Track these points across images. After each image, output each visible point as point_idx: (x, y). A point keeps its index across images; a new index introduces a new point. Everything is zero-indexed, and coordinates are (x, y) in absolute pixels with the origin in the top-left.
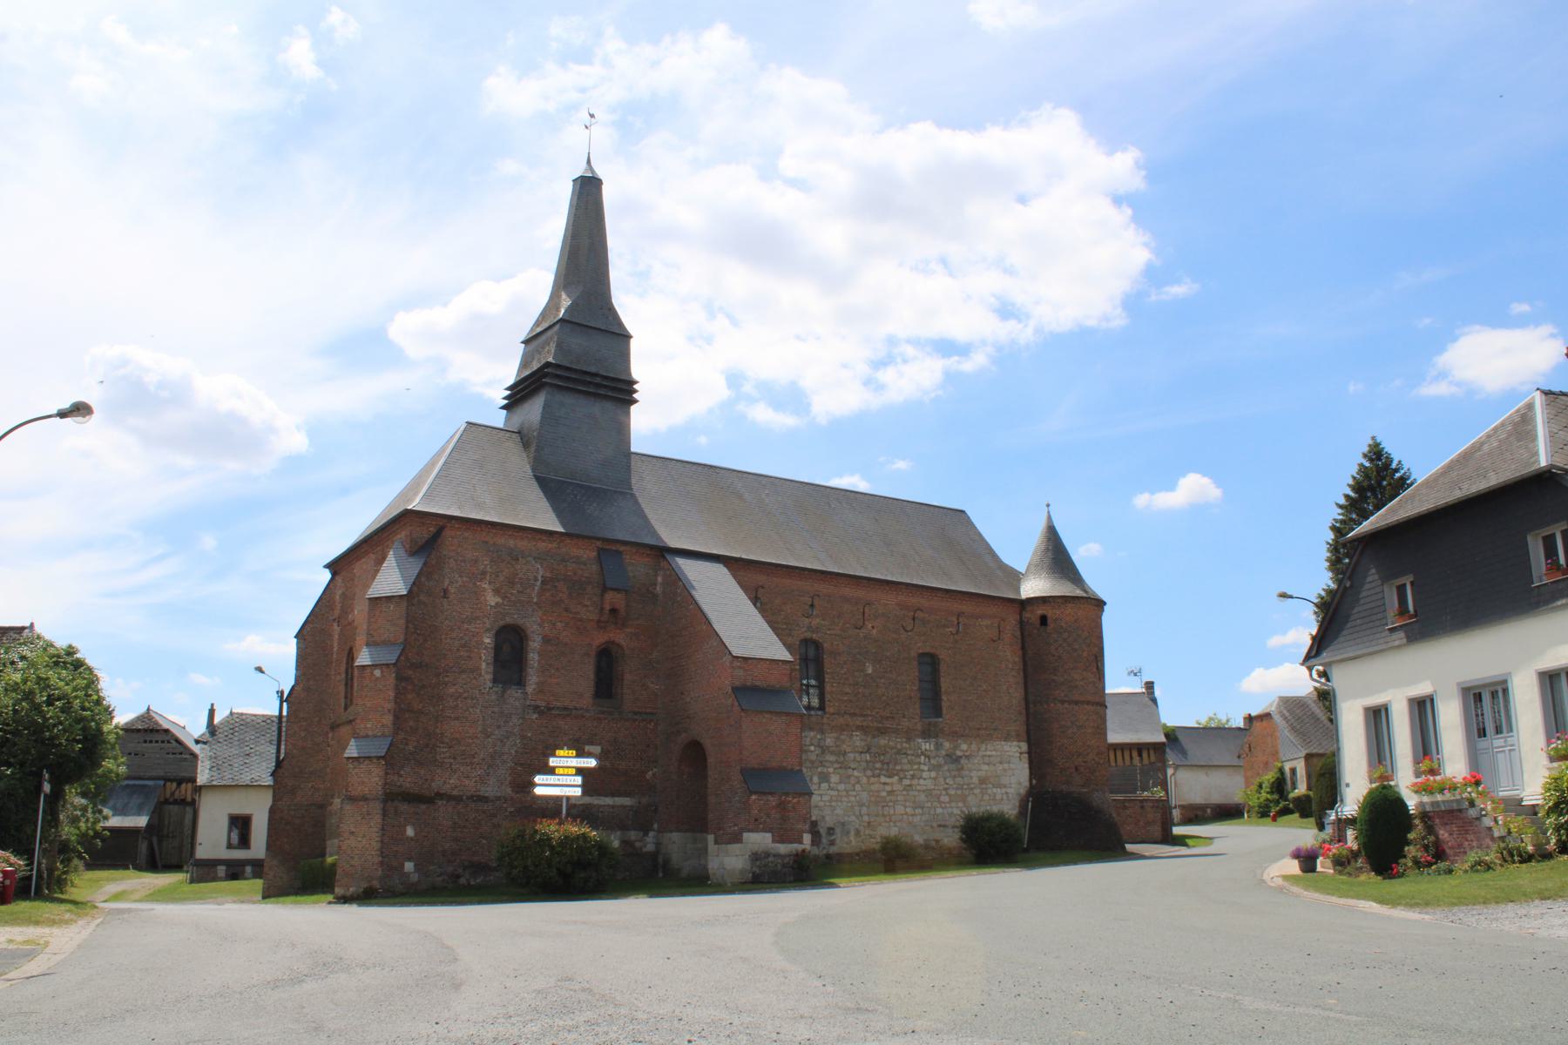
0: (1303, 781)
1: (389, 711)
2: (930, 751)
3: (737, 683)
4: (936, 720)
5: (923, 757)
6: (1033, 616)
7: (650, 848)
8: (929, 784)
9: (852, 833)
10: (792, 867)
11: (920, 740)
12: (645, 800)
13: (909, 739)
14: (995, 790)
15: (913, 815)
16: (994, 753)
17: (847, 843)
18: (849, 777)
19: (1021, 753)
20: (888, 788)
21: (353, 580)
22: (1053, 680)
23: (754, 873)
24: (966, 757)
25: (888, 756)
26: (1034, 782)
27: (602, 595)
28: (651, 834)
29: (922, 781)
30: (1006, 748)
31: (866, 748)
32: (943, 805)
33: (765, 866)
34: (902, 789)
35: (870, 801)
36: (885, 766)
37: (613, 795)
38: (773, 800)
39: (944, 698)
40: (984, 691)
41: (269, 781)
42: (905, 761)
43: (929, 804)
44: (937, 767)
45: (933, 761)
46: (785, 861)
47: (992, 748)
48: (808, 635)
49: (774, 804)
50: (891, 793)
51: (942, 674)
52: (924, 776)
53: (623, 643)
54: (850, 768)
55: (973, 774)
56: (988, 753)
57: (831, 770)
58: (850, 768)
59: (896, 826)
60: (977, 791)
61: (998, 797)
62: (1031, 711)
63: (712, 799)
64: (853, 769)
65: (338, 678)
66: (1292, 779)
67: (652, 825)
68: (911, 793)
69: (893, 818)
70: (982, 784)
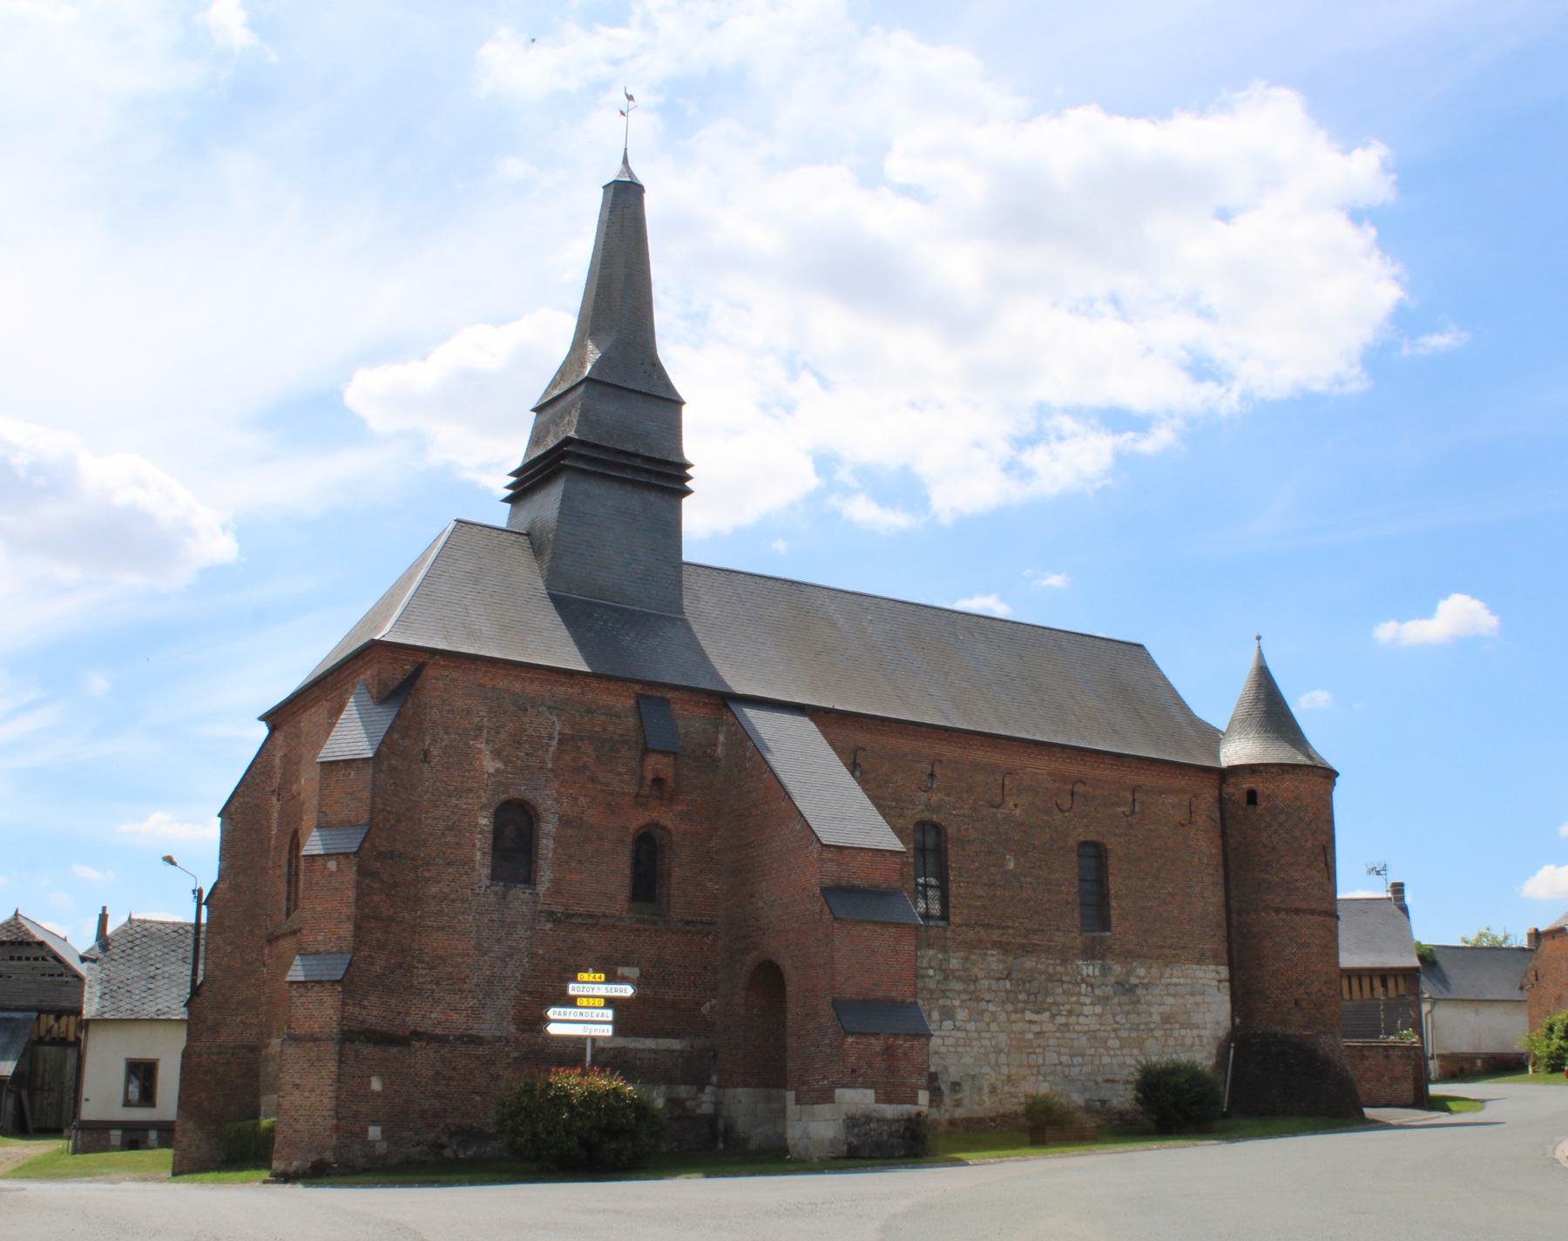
1: (348, 917)
2: (1094, 977)
3: (828, 882)
4: (1104, 934)
5: (1084, 986)
7: (707, 1108)
8: (1093, 1023)
9: (986, 1090)
11: (1080, 962)
13: (1064, 962)
14: (1183, 1032)
15: (1069, 1066)
16: (1182, 981)
17: (979, 1105)
18: (982, 1012)
19: (1220, 981)
20: (1036, 1028)
21: (298, 737)
22: (1265, 880)
24: (1143, 985)
25: (1036, 984)
28: (708, 1089)
29: (1082, 1019)
30: (1200, 974)
31: (1006, 972)
32: (1112, 1052)
33: (866, 1134)
34: (1054, 1029)
36: (1032, 998)
37: (655, 1035)
38: (877, 1044)
39: (1113, 903)
41: (182, 1013)
42: (1060, 990)
44: (1103, 1000)
45: (1097, 992)
46: (893, 1128)
47: (1180, 974)
48: (926, 816)
49: (878, 1049)
50: (1039, 1034)
51: (1111, 871)
53: (670, 825)
54: (983, 999)
56: (1175, 980)
57: (957, 1003)
58: (983, 999)
59: (1045, 1081)
60: (1158, 1033)
61: (1188, 1041)
63: (792, 1043)
64: (988, 1002)
65: (278, 872)
68: (1067, 1035)
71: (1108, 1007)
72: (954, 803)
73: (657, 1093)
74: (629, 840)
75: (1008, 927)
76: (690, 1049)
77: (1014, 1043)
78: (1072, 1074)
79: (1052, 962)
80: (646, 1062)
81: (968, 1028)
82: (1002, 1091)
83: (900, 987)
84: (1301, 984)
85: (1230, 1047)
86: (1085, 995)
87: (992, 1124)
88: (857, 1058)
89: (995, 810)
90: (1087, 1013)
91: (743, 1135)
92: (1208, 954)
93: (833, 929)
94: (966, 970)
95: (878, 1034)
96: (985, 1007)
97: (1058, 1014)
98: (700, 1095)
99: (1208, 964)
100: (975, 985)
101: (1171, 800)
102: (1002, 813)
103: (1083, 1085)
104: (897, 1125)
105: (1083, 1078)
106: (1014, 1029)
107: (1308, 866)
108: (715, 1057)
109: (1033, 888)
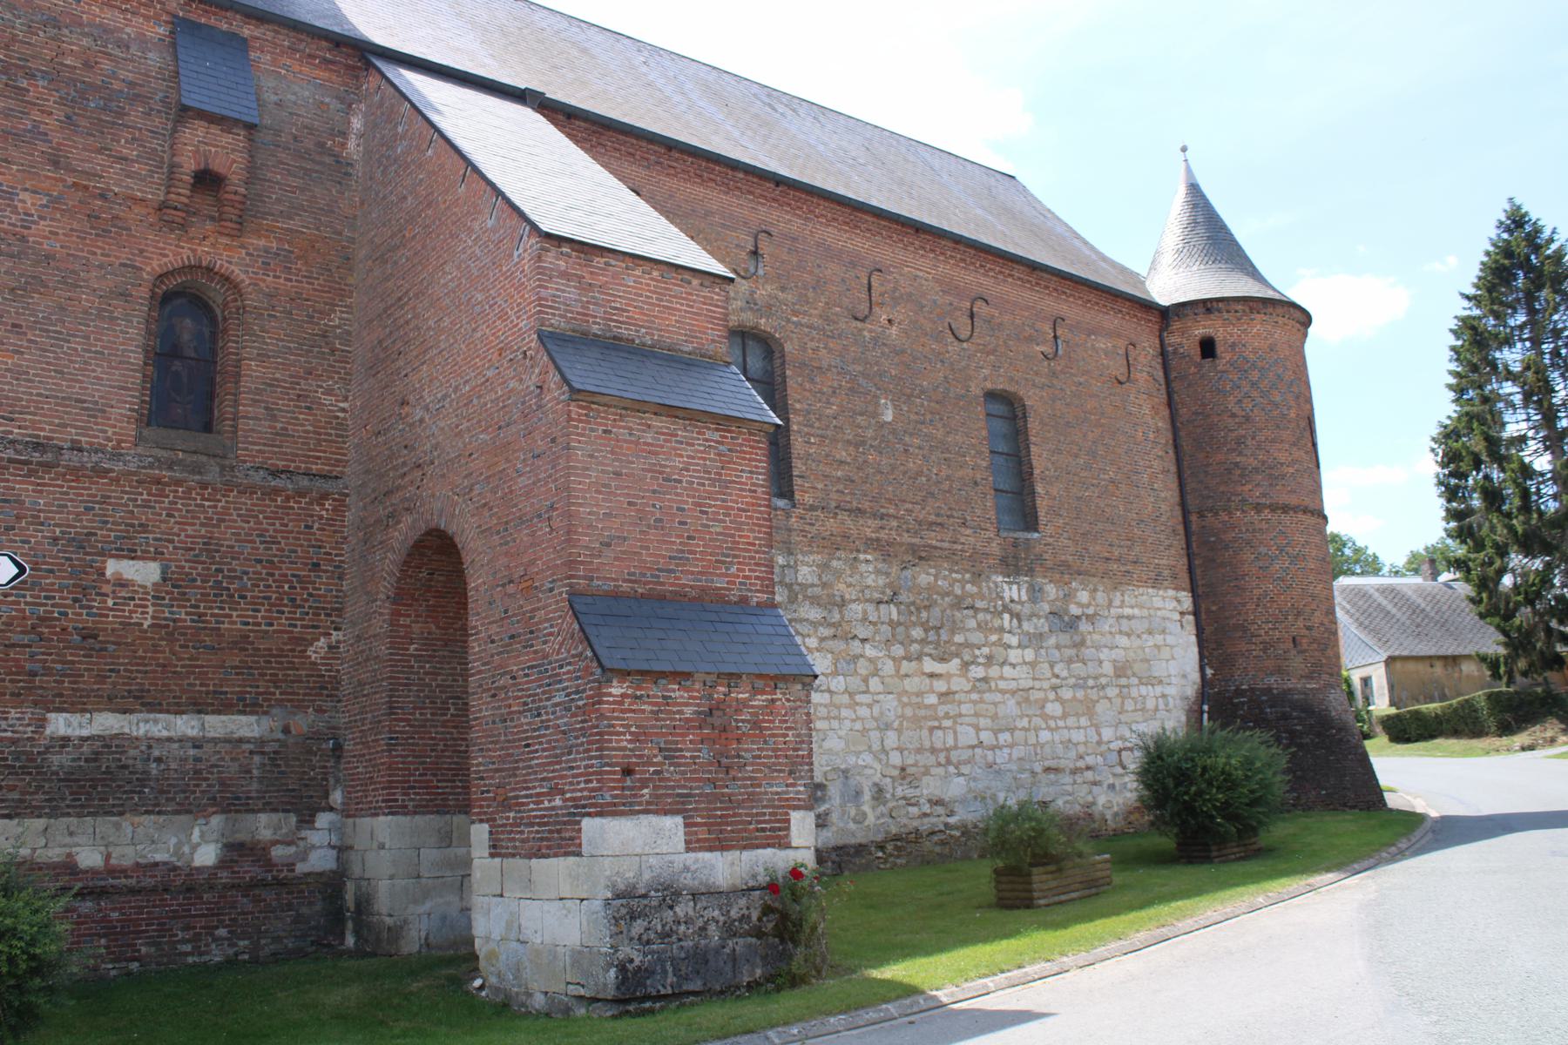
0: (1383, 694)
2: (1020, 602)
3: (557, 322)
4: (1029, 536)
5: (1006, 616)
6: (1186, 338)
7: (320, 860)
8: (1022, 677)
9: (867, 796)
10: (759, 933)
11: (1000, 579)
12: (303, 722)
13: (977, 576)
14: (1144, 691)
15: (993, 748)
16: (1136, 611)
17: (855, 821)
18: (856, 658)
19: (1182, 613)
20: (940, 686)
22: (1236, 464)
23: (622, 968)
24: (1088, 616)
25: (936, 611)
26: (1209, 672)
27: (174, 131)
28: (323, 819)
29: (1007, 670)
30: (1157, 602)
31: (889, 592)
32: (1052, 724)
33: (665, 935)
34: (968, 687)
35: (903, 716)
36: (932, 636)
37: (199, 707)
38: (685, 702)
39: (1039, 489)
40: (1112, 481)
42: (972, 623)
43: (1024, 723)
44: (1036, 640)
45: (1026, 626)
46: (734, 913)
47: (1133, 601)
48: (748, 318)
49: (688, 712)
50: (945, 696)
51: (1033, 439)
52: (1012, 660)
53: (238, 273)
54: (855, 637)
55: (1105, 654)
56: (1128, 611)
58: (855, 637)
59: (960, 775)
60: (1112, 692)
61: (1150, 704)
62: (1194, 527)
63: (482, 708)
64: (864, 641)
66: (1363, 692)
67: (326, 795)
68: (987, 696)
69: (954, 755)
70: (1119, 676)
71: (1043, 652)
72: (794, 304)
73: (202, 835)
74: (144, 292)
75: (888, 515)
76: (281, 736)
77: (909, 712)
78: (998, 761)
79: (958, 576)
80: (173, 766)
81: (833, 688)
82: (893, 795)
83: (733, 570)
84: (1298, 614)
85: (1202, 712)
86: (1010, 632)
87: (880, 854)
88: (636, 738)
89: (859, 324)
90: (1014, 661)
91: (388, 920)
92: (1166, 573)
93: (570, 419)
94: (824, 585)
95: (688, 675)
96: (859, 651)
97: (973, 663)
98: (303, 834)
99: (1167, 588)
100: (840, 612)
101: (1102, 344)
102: (870, 331)
103: (1015, 779)
104: (743, 902)
105: (1014, 767)
106: (908, 688)
107: (1294, 444)
108: (338, 748)
109: (924, 456)
